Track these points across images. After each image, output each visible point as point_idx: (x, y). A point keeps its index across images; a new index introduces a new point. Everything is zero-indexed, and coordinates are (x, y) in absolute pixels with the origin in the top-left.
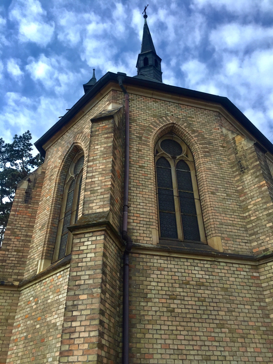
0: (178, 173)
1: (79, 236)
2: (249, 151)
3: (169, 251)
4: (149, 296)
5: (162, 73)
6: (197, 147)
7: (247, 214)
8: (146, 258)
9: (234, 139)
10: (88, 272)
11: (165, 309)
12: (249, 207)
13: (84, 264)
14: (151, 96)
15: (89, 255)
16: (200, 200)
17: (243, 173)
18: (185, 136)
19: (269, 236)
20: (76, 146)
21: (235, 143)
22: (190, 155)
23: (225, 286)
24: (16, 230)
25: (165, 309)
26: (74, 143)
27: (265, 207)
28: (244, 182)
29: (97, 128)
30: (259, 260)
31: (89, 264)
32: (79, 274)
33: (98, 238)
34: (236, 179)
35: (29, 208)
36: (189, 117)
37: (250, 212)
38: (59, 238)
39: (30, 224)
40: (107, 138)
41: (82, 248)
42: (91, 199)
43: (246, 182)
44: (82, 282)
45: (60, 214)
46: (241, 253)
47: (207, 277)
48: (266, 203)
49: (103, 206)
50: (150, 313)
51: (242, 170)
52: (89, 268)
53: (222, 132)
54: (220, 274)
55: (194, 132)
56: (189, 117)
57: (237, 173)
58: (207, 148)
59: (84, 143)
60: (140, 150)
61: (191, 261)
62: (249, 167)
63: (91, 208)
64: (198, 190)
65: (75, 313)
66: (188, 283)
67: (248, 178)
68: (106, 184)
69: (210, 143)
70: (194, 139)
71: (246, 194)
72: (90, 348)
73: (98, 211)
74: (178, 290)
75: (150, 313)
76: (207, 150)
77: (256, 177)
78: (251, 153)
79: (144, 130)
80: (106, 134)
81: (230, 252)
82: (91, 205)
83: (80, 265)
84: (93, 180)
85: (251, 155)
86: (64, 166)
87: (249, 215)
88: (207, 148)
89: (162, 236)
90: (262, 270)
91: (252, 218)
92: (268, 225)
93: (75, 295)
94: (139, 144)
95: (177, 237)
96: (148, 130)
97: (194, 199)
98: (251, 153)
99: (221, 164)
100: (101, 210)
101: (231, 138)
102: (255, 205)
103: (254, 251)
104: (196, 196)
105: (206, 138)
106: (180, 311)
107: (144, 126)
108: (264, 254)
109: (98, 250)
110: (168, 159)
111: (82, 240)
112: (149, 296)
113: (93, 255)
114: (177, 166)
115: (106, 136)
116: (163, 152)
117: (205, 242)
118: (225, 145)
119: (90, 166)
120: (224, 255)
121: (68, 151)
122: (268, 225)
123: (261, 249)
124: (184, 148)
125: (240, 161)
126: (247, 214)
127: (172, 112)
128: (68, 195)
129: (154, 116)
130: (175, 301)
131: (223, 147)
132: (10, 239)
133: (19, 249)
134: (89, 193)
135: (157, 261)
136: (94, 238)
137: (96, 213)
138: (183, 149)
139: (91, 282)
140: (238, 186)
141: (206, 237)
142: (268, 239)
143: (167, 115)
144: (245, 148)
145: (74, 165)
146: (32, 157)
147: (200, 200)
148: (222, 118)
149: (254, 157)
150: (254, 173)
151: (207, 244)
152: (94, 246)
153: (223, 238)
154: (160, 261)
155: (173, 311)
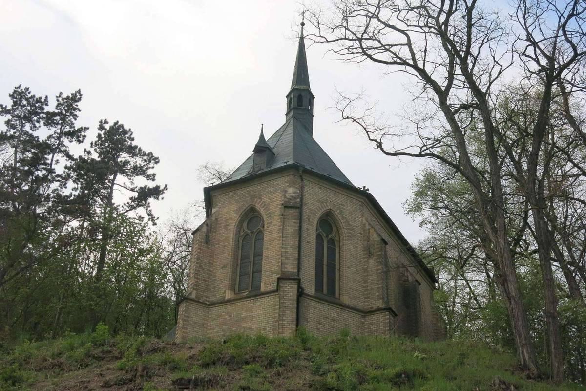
0: (328, 248)
1: (283, 283)
2: (377, 243)
3: (320, 299)
4: (309, 320)
5: (313, 116)
6: (344, 231)
7: (366, 285)
8: (308, 301)
9: (369, 229)
10: (290, 302)
11: (315, 328)
12: (369, 281)
13: (287, 297)
14: (317, 183)
15: (290, 294)
16: (339, 270)
17: (370, 257)
18: (338, 223)
19: (375, 300)
20: (252, 207)
21: (369, 233)
22: (337, 235)
23: (346, 323)
24: (202, 265)
25: (315, 328)
26: (251, 204)
27: (377, 283)
28: (369, 263)
29: (288, 213)
30: (366, 313)
31: (290, 298)
32: (285, 301)
33: (294, 286)
34: (364, 260)
35: (209, 248)
36: (342, 205)
37: (369, 284)
38: (238, 277)
39: (211, 262)
40: (295, 223)
41: (285, 289)
42: (286, 262)
43: (370, 264)
44: (287, 306)
45: (237, 260)
46: (357, 307)
47: (337, 316)
48: (379, 280)
49: (293, 268)
50: (308, 328)
51: (370, 255)
52: (290, 300)
53: (362, 220)
54: (345, 317)
55: (343, 218)
56: (342, 205)
57: (366, 256)
58: (350, 233)
59: (264, 210)
60: (308, 230)
61: (330, 307)
62: (375, 254)
63: (286, 268)
64: (340, 263)
65: (284, 318)
66: (327, 318)
67: (372, 262)
68: (295, 255)
69: (352, 230)
70: (343, 224)
71: (368, 272)
72: (292, 332)
73: (290, 270)
74: (322, 320)
75: (308, 328)
76: (350, 235)
77: (377, 262)
78: (378, 245)
79: (311, 213)
80: (295, 219)
81: (352, 305)
82: (286, 266)
83: (285, 297)
84: (287, 250)
85: (377, 246)
86: (240, 221)
87: (367, 286)
88: (350, 233)
89: (316, 290)
90: (367, 318)
91: (369, 288)
92: (376, 294)
93: (283, 310)
94: (308, 224)
95: (323, 291)
96: (314, 213)
97: (335, 269)
98: (378, 245)
99: (357, 247)
100: (292, 270)
101: (367, 228)
102: (372, 280)
103: (365, 307)
104: (337, 267)
105: (350, 225)
106: (322, 330)
107: (312, 210)
108: (371, 310)
109: (294, 292)
110: (323, 237)
111: (285, 285)
112: (309, 320)
113: (291, 294)
114: (328, 242)
115: (294, 221)
116: (321, 230)
117: (338, 298)
118: (362, 232)
119: (285, 241)
120: (348, 307)
121: (245, 209)
122: (376, 294)
123: (369, 307)
124: (334, 228)
125: (369, 248)
126: (366, 285)
127: (330, 199)
128: (242, 246)
129: (319, 201)
130: (321, 325)
131: (360, 233)
132: (199, 271)
133: (206, 279)
134: (284, 258)
135: (314, 303)
136: (292, 286)
137: (289, 272)
138: (333, 229)
139: (291, 306)
140: (365, 265)
141: (340, 294)
142: (374, 302)
143: (327, 201)
144: (375, 240)
145: (247, 221)
146: (74, 127)
147: (339, 270)
148: (365, 207)
149: (379, 248)
150: (377, 259)
151: (339, 299)
152: (292, 290)
153: (349, 297)
154: (315, 304)
155: (319, 329)
